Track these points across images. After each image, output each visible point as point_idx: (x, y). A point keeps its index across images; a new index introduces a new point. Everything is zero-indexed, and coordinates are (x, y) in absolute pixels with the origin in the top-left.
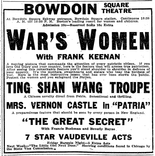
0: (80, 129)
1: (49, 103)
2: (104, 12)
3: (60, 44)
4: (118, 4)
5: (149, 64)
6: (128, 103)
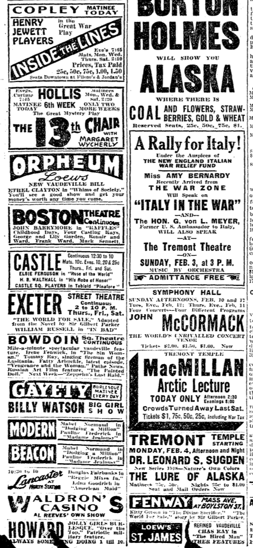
3: (195, 73)
4: (209, 291)
6: (146, 201)
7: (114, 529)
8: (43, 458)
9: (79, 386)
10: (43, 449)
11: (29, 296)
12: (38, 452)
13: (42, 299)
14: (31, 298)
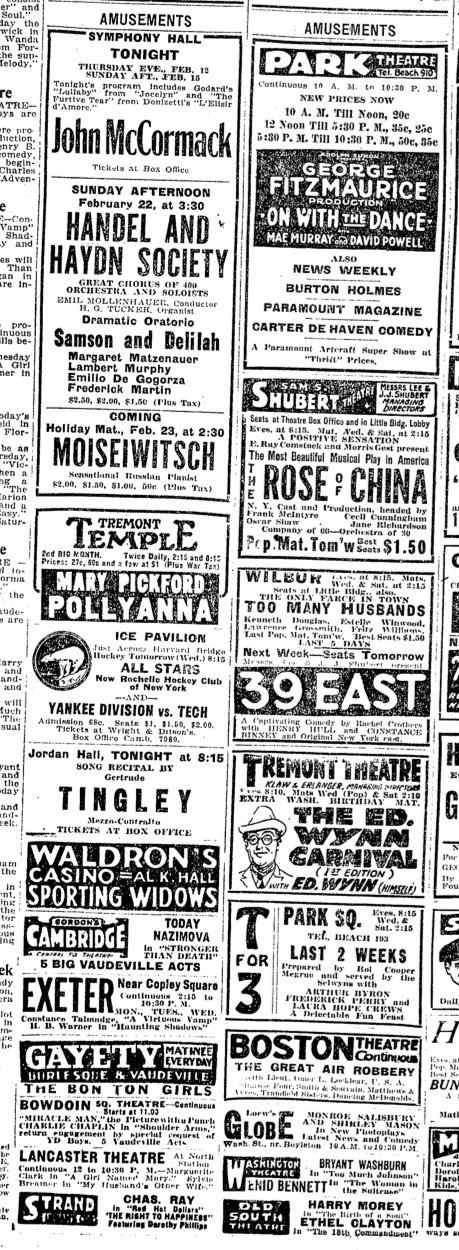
0: (300, 327)
5: (215, 987)
7: (132, 381)
9: (144, 1049)
11: (60, 980)
13: (82, 987)
14: (62, 984)
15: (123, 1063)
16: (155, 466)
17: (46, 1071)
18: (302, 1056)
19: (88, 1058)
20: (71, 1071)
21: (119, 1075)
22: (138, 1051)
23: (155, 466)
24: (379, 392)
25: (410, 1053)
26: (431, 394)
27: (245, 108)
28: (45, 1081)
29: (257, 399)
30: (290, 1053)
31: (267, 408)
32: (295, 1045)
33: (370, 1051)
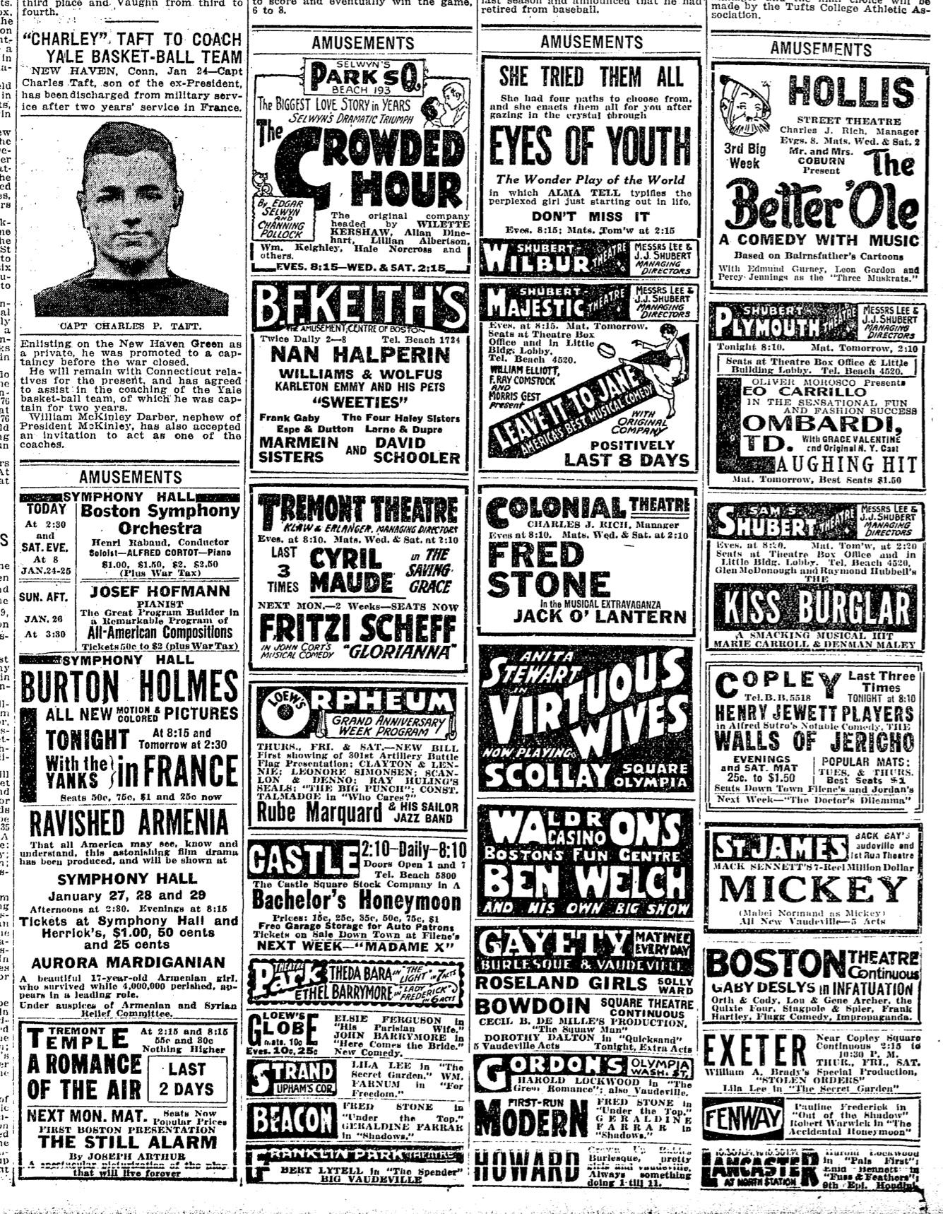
1: (578, 1132)
2: (44, 1145)
8: (312, 1129)
9: (612, 935)
10: (312, 1111)
12: (303, 1117)
15: (590, 951)
16: (664, 162)
17: (501, 958)
18: (788, 973)
19: (550, 943)
20: (530, 959)
21: (585, 964)
22: (606, 936)
23: (664, 162)
24: (860, 515)
25: (911, 969)
26: (919, 515)
27: (706, 204)
28: (502, 971)
29: (723, 526)
30: (774, 970)
31: (734, 536)
32: (779, 960)
33: (864, 966)
